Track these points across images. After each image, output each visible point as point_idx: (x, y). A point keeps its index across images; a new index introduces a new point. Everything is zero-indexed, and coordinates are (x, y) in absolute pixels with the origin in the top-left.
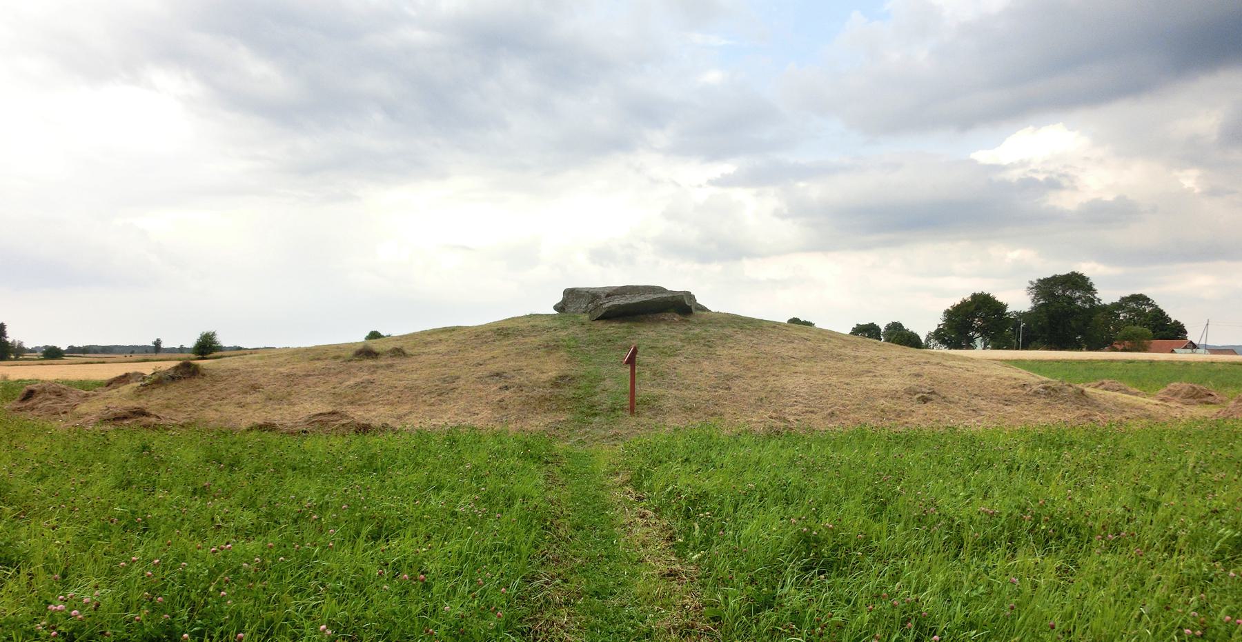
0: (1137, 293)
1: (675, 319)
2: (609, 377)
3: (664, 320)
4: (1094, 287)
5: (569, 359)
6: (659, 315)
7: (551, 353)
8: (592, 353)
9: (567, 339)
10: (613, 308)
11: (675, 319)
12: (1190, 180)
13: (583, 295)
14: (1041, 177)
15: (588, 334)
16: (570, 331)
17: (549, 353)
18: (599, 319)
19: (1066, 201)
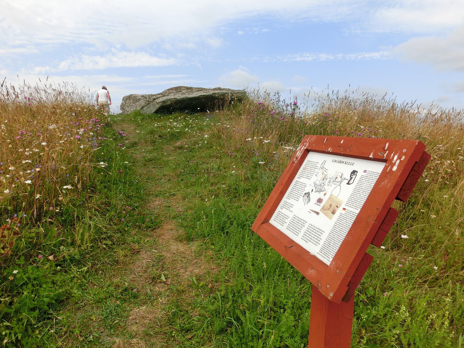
10: (169, 103)
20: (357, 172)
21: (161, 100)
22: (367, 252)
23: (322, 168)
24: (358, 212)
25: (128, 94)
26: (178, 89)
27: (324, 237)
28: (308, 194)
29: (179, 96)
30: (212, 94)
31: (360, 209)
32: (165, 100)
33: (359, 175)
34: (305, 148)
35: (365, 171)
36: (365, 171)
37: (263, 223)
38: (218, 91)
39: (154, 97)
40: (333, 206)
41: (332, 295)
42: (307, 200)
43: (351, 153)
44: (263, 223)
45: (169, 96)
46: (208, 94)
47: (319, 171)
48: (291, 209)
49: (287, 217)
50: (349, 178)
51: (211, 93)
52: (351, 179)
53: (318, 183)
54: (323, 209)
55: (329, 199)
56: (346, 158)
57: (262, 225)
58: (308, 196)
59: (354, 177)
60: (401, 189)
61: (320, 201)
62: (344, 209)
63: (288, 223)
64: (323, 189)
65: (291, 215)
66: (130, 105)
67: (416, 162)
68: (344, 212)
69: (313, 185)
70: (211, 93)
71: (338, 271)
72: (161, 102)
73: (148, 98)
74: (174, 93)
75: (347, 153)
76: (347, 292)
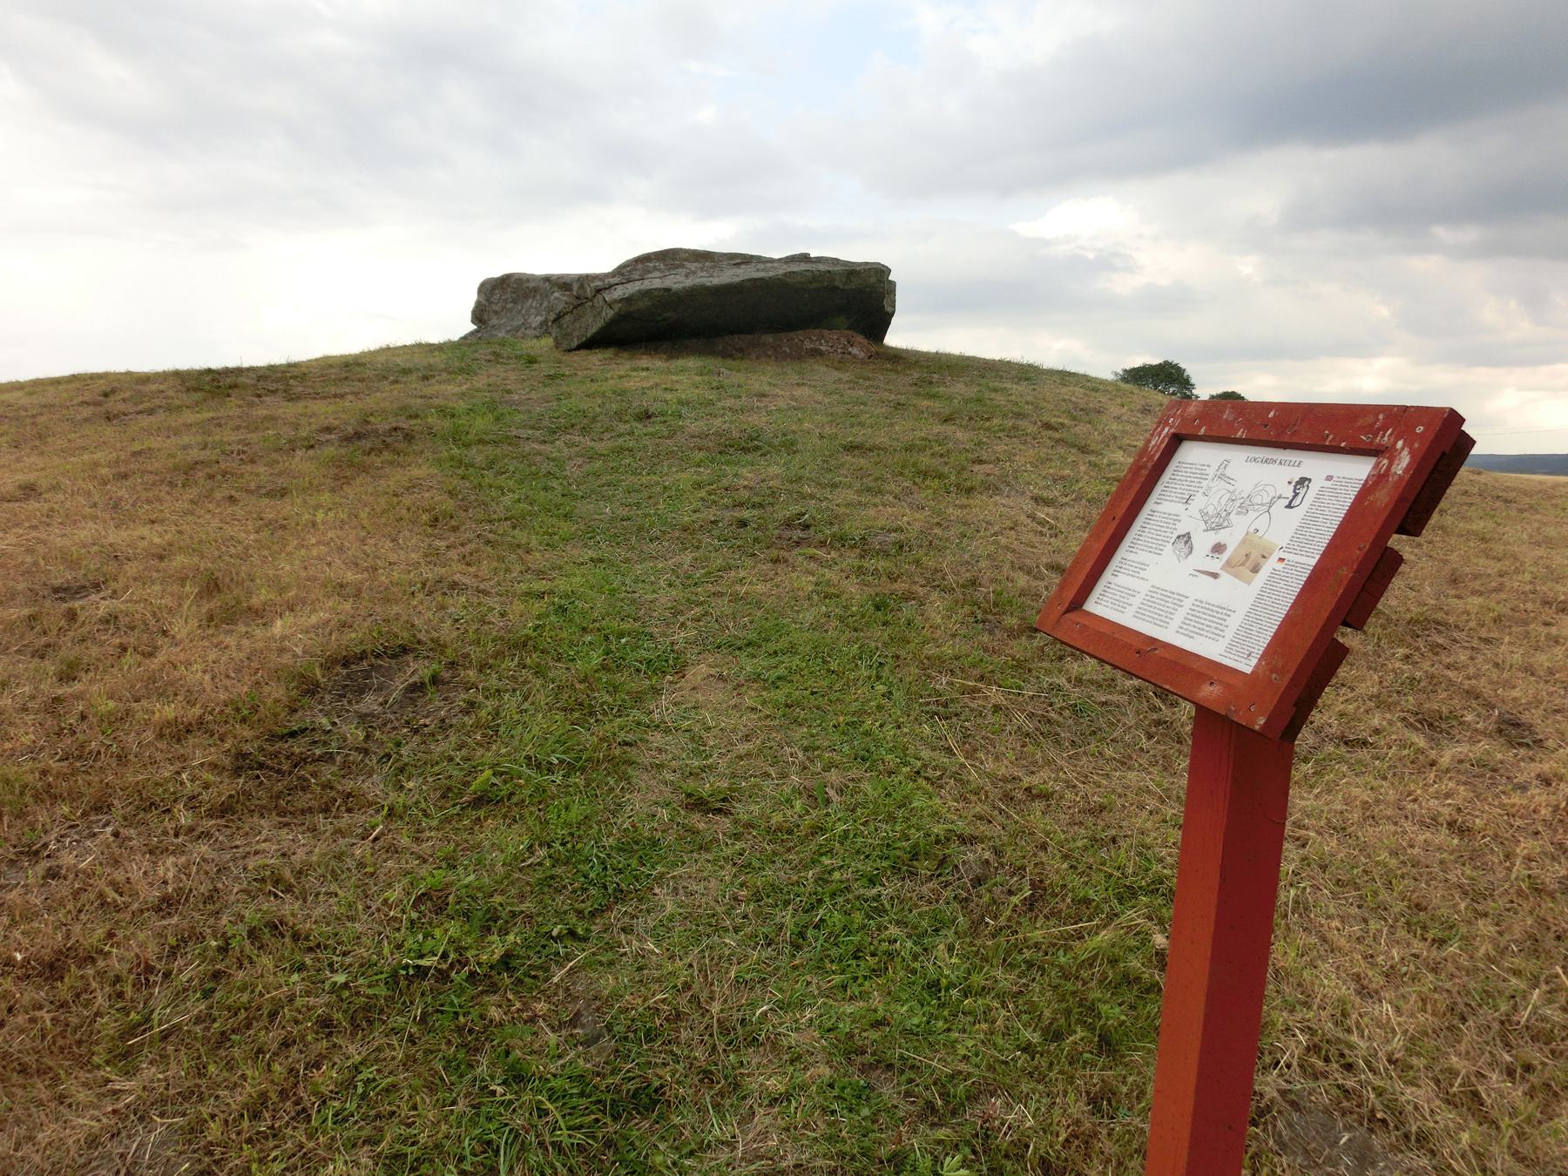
0: (1230, 390)
1: (855, 351)
2: (705, 645)
3: (816, 353)
4: (1192, 381)
5: (449, 505)
6: (798, 336)
7: (364, 469)
8: (571, 470)
9: (462, 405)
10: (644, 304)
11: (855, 351)
12: (1248, 267)
13: (535, 290)
14: (1091, 256)
15: (549, 391)
16: (480, 382)
17: (343, 472)
18: (590, 344)
19: (1122, 285)
20: (1310, 480)
21: (619, 293)
22: (1389, 544)
23: (1222, 477)
24: (1313, 562)
25: (497, 272)
26: (670, 258)
27: (1234, 622)
28: (1186, 537)
29: (677, 281)
30: (785, 274)
31: (1318, 557)
32: (632, 295)
33: (1314, 488)
34: (1172, 430)
35: (1329, 478)
36: (1329, 478)
37: (1068, 611)
38: (803, 267)
39: (599, 283)
40: (1252, 557)
41: (1262, 722)
42: (1186, 550)
43: (1294, 440)
44: (1068, 611)
45: (646, 282)
46: (771, 274)
47: (1211, 485)
48: (1142, 574)
49: (1133, 593)
50: (1291, 494)
51: (782, 270)
52: (1294, 497)
53: (1211, 511)
54: (1229, 565)
55: (1244, 541)
56: (1288, 451)
57: (1067, 615)
58: (1186, 542)
59: (1302, 491)
60: (1410, 510)
61: (1218, 548)
62: (1281, 560)
63: (1134, 608)
64: (1226, 524)
65: (1143, 588)
66: (503, 308)
67: (1444, 454)
68: (1280, 566)
69: (1199, 516)
70: (781, 272)
71: (1274, 676)
72: (621, 300)
73: (575, 287)
74: (659, 270)
75: (1286, 439)
76: (1293, 718)
